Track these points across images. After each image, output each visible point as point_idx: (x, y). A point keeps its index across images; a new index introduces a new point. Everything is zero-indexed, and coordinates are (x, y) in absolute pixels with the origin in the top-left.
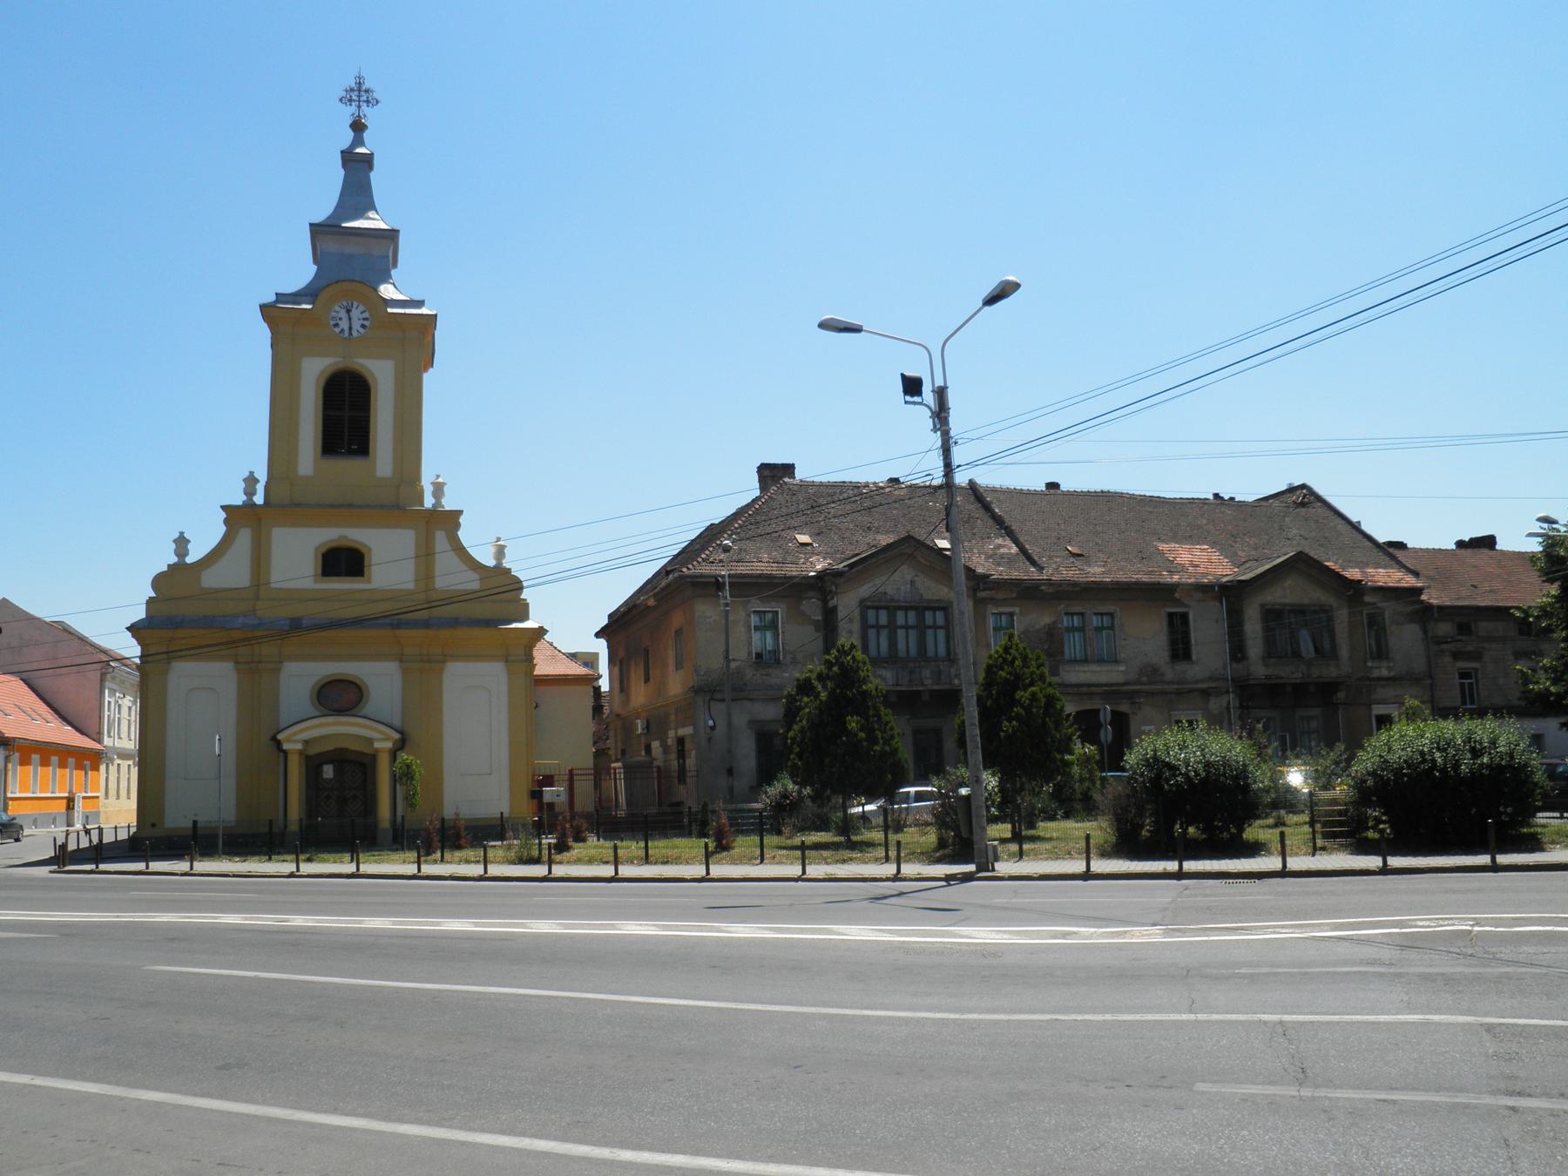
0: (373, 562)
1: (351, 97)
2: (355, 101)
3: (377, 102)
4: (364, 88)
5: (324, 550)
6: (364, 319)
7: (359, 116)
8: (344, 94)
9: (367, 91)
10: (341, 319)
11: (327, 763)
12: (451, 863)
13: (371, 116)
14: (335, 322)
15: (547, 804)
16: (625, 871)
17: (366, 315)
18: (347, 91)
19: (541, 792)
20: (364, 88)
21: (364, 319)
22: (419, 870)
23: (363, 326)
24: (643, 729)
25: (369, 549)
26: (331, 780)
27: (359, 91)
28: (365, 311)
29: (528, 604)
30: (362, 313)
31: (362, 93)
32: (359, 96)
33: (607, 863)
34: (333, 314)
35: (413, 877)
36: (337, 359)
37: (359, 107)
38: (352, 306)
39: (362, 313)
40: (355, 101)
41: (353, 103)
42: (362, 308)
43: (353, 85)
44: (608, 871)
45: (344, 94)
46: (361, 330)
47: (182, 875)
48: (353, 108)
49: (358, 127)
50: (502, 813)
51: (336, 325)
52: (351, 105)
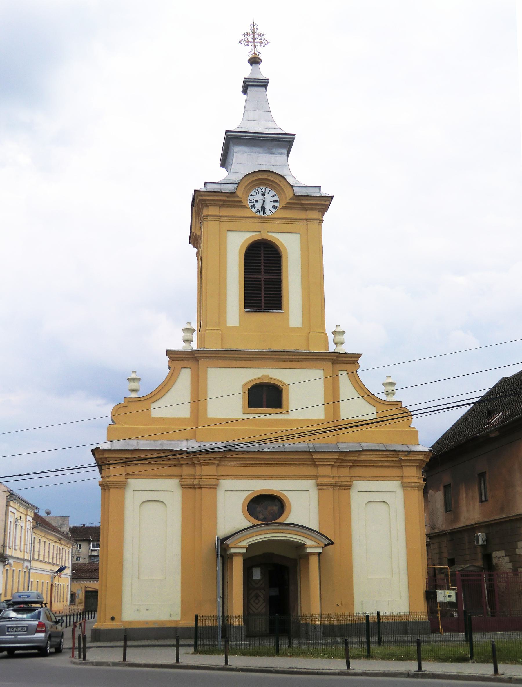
0: (241, 395)
1: (248, 39)
2: (250, 42)
3: (268, 43)
4: (257, 33)
5: (250, 386)
6: (275, 201)
7: (255, 53)
8: (243, 37)
9: (260, 35)
10: (256, 201)
11: (256, 566)
12: (285, 655)
13: (263, 53)
14: (252, 204)
15: (440, 603)
16: (429, 667)
17: (276, 198)
18: (244, 35)
19: (435, 594)
20: (257, 33)
21: (275, 201)
22: (348, 666)
23: (274, 207)
24: (484, 541)
25: (244, 385)
26: (260, 580)
27: (254, 34)
28: (275, 195)
29: (417, 431)
30: (273, 197)
31: (256, 36)
32: (254, 39)
33: (411, 659)
34: (251, 198)
35: (415, 676)
36: (252, 234)
37: (254, 46)
38: (265, 192)
39: (273, 197)
40: (250, 42)
41: (249, 44)
42: (272, 193)
43: (250, 31)
44: (412, 666)
45: (243, 37)
46: (274, 210)
47: (339, 674)
48: (250, 48)
49: (254, 61)
50: (378, 613)
51: (253, 206)
52: (248, 45)
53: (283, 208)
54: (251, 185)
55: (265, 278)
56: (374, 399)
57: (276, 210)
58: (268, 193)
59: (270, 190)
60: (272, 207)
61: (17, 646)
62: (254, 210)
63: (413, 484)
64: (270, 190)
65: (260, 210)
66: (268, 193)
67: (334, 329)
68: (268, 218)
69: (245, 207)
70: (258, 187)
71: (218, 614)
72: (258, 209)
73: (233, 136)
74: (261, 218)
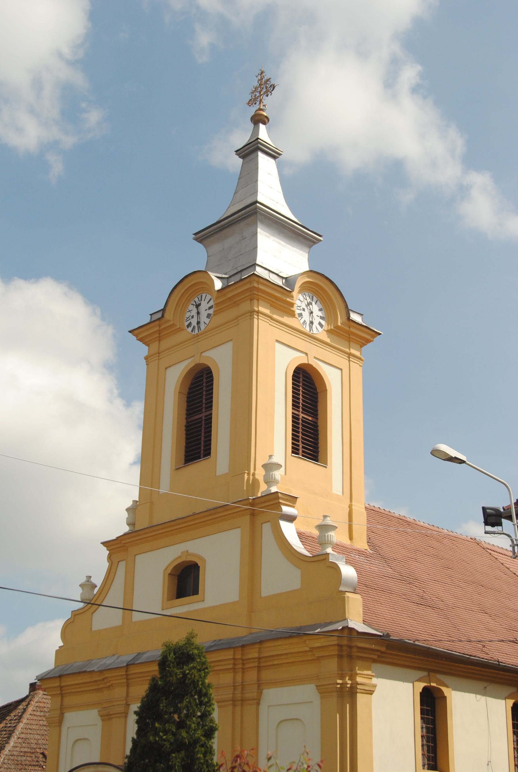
51: (189, 325)
53: (216, 313)
54: (311, 286)
55: (303, 417)
56: (306, 561)
57: (210, 320)
58: (204, 301)
59: (206, 295)
60: (207, 317)
61: (350, 766)
62: (190, 329)
63: (328, 687)
64: (206, 295)
65: (306, 323)
66: (204, 301)
67: (266, 461)
68: (205, 332)
69: (180, 330)
70: (194, 297)
71: (228, 703)
72: (194, 326)
73: (288, 225)
74: (197, 335)
